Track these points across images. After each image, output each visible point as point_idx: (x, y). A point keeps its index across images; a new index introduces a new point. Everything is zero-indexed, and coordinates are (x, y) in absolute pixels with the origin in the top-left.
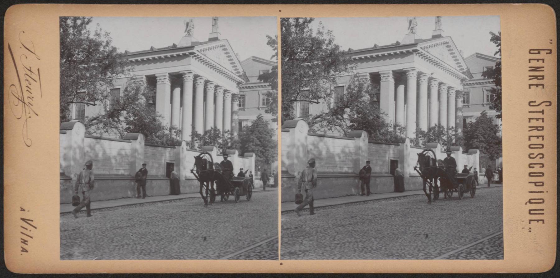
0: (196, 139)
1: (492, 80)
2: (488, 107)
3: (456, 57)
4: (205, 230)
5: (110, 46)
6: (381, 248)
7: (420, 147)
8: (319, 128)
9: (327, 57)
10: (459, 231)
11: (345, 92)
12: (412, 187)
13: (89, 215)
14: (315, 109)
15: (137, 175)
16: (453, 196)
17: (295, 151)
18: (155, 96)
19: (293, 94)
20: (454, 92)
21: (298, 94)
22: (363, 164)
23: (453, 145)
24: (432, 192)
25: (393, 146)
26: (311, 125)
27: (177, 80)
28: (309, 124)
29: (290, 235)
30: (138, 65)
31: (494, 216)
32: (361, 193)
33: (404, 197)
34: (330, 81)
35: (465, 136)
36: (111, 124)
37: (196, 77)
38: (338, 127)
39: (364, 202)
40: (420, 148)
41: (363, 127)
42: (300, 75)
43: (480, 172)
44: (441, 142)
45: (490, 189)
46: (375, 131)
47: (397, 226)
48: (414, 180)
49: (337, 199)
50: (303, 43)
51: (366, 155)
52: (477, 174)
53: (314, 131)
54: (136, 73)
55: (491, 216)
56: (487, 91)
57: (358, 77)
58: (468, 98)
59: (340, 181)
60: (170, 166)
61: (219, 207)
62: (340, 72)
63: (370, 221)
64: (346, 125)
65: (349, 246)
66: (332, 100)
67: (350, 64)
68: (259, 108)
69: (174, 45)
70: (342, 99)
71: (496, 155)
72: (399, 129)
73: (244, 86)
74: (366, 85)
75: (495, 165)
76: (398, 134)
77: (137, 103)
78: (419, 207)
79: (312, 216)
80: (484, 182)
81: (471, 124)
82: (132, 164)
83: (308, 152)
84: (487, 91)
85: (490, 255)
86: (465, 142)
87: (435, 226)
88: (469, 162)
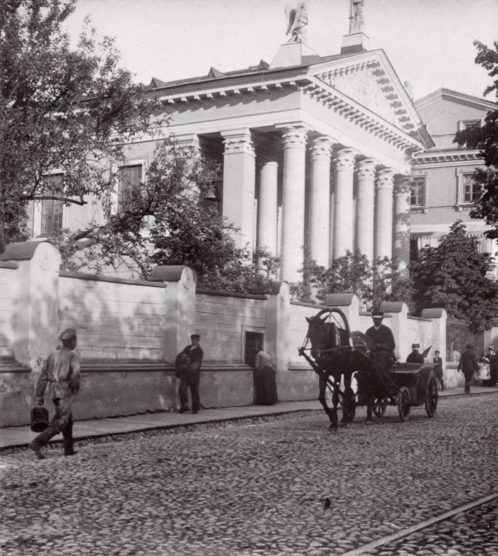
0: (313, 277)
1: (477, 152)
2: (468, 212)
3: (396, 97)
4: (329, 484)
5: (115, 69)
6: (225, 530)
7: (313, 302)
8: (86, 260)
9: (103, 98)
10: (400, 492)
11: (144, 179)
12: (294, 392)
13: (69, 451)
14: (76, 218)
15: (180, 359)
16: (386, 414)
17: (29, 312)
18: (221, 182)
19: (26, 182)
20: (390, 177)
21: (37, 183)
22: (183, 343)
23: (387, 298)
24: (339, 405)
25: (252, 301)
26: (66, 252)
27: (269, 145)
28: (62, 250)
29: (20, 502)
30: (181, 112)
31: (479, 460)
32: (178, 407)
33: (276, 415)
34: (109, 153)
35: (415, 279)
36: (119, 245)
37: (313, 137)
38: (127, 258)
39: (186, 426)
40: (312, 304)
41: (183, 259)
42: (43, 140)
43: (449, 359)
44: (359, 291)
45: (470, 399)
46: (211, 267)
47: (262, 481)
48: (298, 377)
49: (125, 420)
50: (48, 67)
51: (190, 321)
52: (440, 366)
53: (73, 267)
54: (177, 130)
55: (473, 459)
56: (466, 175)
57: (172, 143)
58: (422, 191)
59: (133, 380)
60: (253, 340)
61: (363, 432)
62: (133, 133)
63: (201, 470)
64: (146, 254)
65: (152, 527)
66: (115, 198)
67: (156, 115)
68: (456, 208)
69: (263, 65)
70: (136, 193)
71: (484, 322)
72: (265, 263)
73: (424, 157)
74: (190, 163)
75: (482, 343)
76: (263, 273)
77: (178, 197)
78: (311, 438)
79: (70, 459)
80: (455, 382)
81: (429, 251)
82: (168, 337)
83: (60, 315)
84: (466, 175)
85: (468, 546)
86: (414, 291)
87: (347, 480)
88: (422, 336)
